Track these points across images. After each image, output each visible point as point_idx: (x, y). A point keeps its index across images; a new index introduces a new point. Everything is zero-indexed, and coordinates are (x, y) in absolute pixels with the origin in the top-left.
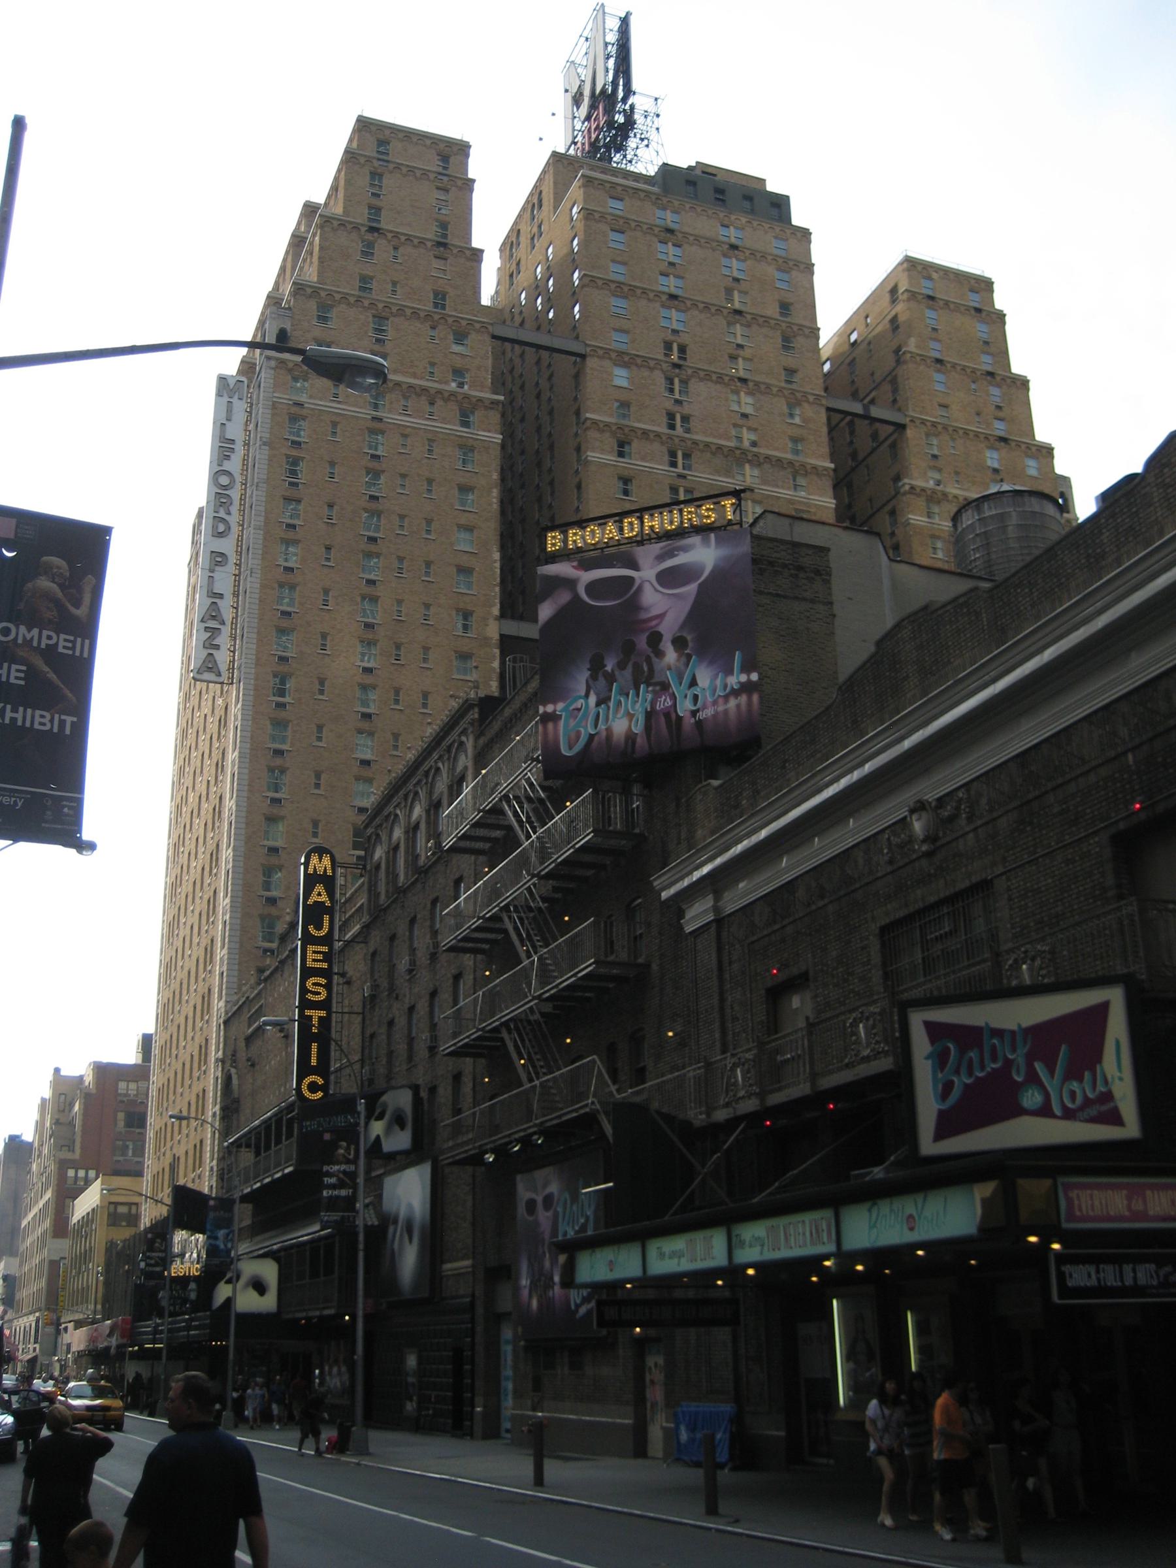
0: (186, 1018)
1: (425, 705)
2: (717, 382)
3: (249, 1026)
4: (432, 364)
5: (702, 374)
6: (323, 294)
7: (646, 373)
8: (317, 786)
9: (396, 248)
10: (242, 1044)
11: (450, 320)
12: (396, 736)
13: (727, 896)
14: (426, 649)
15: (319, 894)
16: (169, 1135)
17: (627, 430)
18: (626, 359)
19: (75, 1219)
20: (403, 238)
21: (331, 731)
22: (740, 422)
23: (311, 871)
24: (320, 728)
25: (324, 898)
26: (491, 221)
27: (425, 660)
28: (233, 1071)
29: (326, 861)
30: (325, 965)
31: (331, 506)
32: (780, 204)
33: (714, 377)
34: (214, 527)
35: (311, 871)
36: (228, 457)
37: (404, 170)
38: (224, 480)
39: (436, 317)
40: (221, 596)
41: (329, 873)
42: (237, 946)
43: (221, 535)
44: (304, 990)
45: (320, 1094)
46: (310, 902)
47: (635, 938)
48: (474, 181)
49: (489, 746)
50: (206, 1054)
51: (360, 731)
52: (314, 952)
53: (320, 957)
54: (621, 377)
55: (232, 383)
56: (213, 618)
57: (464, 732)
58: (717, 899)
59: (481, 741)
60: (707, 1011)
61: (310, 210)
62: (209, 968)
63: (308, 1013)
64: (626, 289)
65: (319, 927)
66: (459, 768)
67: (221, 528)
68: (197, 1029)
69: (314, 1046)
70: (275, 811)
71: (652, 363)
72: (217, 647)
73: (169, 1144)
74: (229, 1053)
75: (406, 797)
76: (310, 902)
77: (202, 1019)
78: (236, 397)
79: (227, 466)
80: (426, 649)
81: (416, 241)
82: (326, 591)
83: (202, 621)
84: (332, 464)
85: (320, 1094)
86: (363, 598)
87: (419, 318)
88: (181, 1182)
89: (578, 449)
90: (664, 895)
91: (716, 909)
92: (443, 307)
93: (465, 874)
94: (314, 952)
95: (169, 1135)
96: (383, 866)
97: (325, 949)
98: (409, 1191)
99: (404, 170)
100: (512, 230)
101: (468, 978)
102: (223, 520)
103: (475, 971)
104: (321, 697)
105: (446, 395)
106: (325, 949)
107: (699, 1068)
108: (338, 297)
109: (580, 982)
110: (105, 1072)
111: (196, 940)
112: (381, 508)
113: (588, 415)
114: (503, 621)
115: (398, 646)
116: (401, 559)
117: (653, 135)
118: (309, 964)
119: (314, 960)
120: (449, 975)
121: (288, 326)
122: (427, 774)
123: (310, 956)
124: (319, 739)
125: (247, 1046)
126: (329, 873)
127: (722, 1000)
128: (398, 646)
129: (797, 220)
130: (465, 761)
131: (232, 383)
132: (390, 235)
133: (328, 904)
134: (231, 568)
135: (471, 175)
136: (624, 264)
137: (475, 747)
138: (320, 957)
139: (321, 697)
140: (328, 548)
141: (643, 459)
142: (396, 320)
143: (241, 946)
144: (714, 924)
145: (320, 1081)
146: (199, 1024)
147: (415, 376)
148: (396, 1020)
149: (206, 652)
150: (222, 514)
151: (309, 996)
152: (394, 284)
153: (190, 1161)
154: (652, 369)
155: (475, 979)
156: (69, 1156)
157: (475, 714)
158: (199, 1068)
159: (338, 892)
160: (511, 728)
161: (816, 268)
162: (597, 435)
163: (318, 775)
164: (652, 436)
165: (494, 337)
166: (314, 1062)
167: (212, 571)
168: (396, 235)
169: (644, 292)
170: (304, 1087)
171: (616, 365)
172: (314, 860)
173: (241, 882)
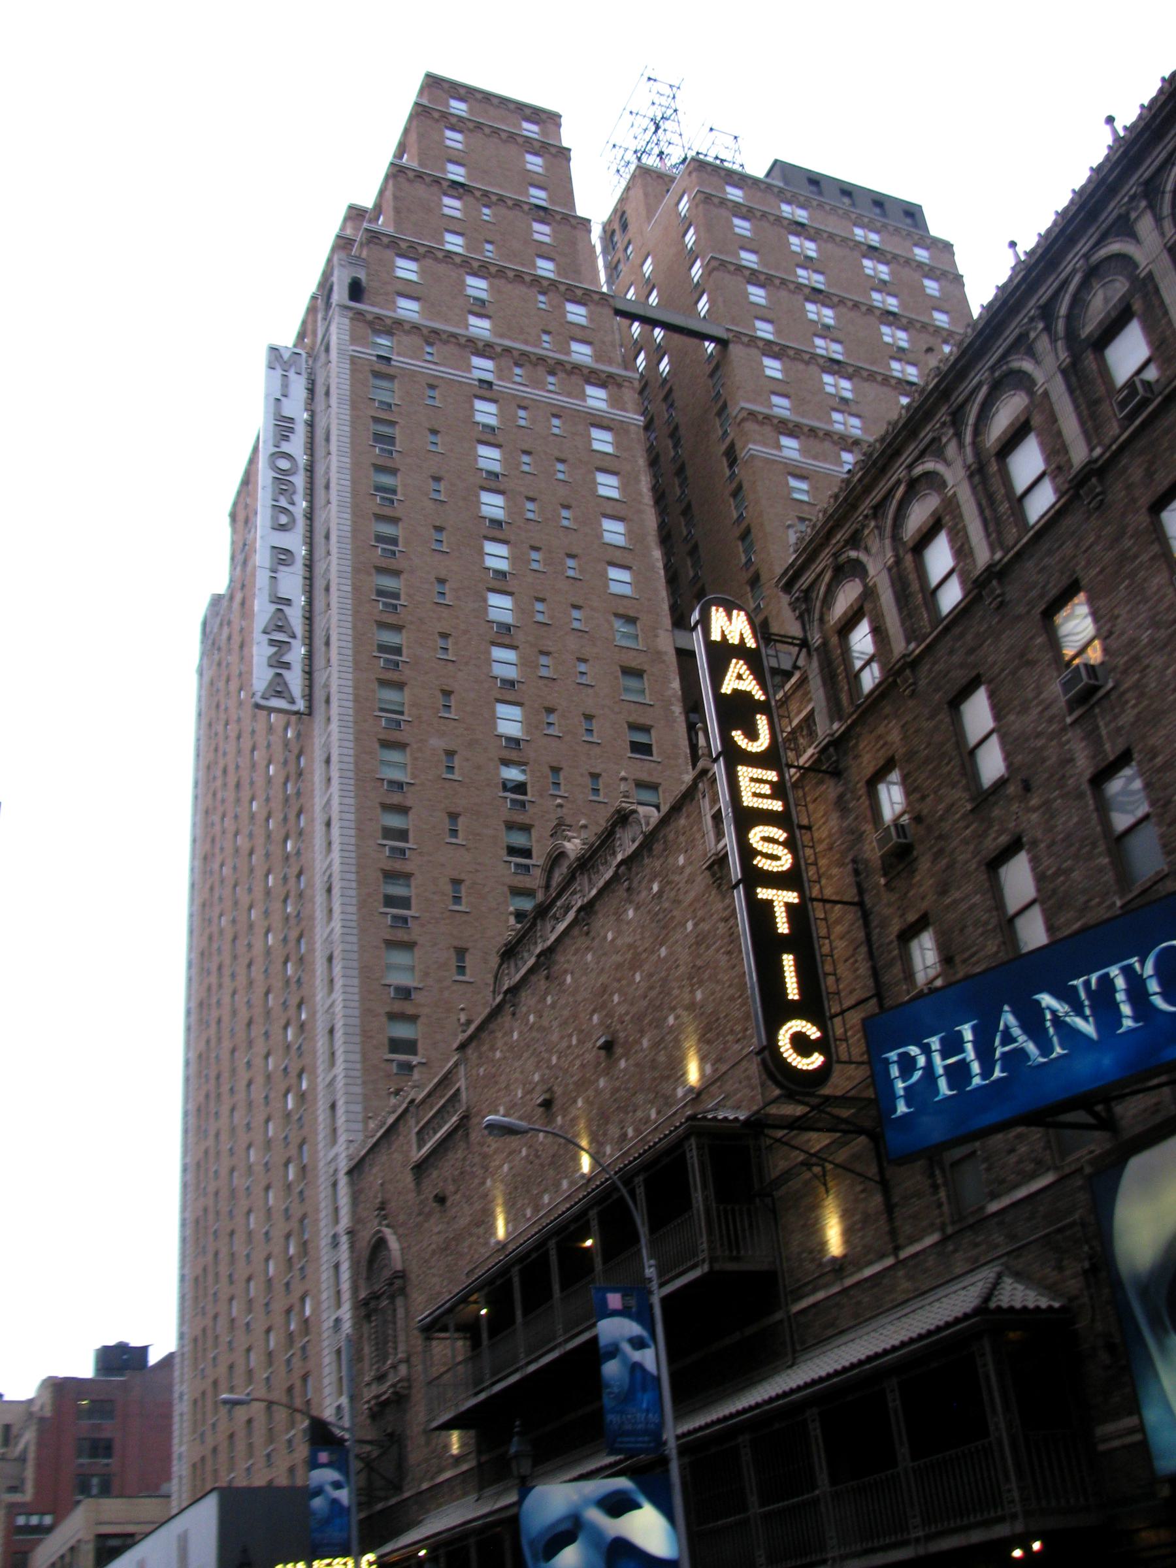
3: (421, 1143)
7: (801, 367)
8: (454, 832)
12: (556, 770)
15: (739, 677)
18: (776, 349)
32: (912, 214)
33: (879, 378)
34: (274, 518)
36: (286, 438)
37: (487, 131)
38: (284, 464)
40: (288, 602)
42: (357, 1057)
43: (282, 528)
45: (816, 1061)
48: (569, 150)
55: (286, 356)
56: (280, 629)
61: (355, 214)
63: (763, 893)
65: (753, 735)
67: (284, 519)
69: (788, 960)
70: (398, 866)
71: (806, 357)
72: (287, 666)
78: (293, 370)
79: (285, 447)
83: (265, 632)
85: (816, 1061)
94: (752, 780)
100: (615, 211)
102: (284, 510)
105: (568, 367)
107: (621, 1443)
110: (61, 1389)
112: (403, 678)
119: (755, 795)
121: (362, 275)
131: (286, 356)
134: (299, 567)
135: (565, 144)
145: (813, 1033)
147: (526, 342)
150: (283, 503)
154: (807, 363)
156: (17, 1498)
162: (756, 427)
166: (793, 991)
171: (764, 355)
173: (355, 964)
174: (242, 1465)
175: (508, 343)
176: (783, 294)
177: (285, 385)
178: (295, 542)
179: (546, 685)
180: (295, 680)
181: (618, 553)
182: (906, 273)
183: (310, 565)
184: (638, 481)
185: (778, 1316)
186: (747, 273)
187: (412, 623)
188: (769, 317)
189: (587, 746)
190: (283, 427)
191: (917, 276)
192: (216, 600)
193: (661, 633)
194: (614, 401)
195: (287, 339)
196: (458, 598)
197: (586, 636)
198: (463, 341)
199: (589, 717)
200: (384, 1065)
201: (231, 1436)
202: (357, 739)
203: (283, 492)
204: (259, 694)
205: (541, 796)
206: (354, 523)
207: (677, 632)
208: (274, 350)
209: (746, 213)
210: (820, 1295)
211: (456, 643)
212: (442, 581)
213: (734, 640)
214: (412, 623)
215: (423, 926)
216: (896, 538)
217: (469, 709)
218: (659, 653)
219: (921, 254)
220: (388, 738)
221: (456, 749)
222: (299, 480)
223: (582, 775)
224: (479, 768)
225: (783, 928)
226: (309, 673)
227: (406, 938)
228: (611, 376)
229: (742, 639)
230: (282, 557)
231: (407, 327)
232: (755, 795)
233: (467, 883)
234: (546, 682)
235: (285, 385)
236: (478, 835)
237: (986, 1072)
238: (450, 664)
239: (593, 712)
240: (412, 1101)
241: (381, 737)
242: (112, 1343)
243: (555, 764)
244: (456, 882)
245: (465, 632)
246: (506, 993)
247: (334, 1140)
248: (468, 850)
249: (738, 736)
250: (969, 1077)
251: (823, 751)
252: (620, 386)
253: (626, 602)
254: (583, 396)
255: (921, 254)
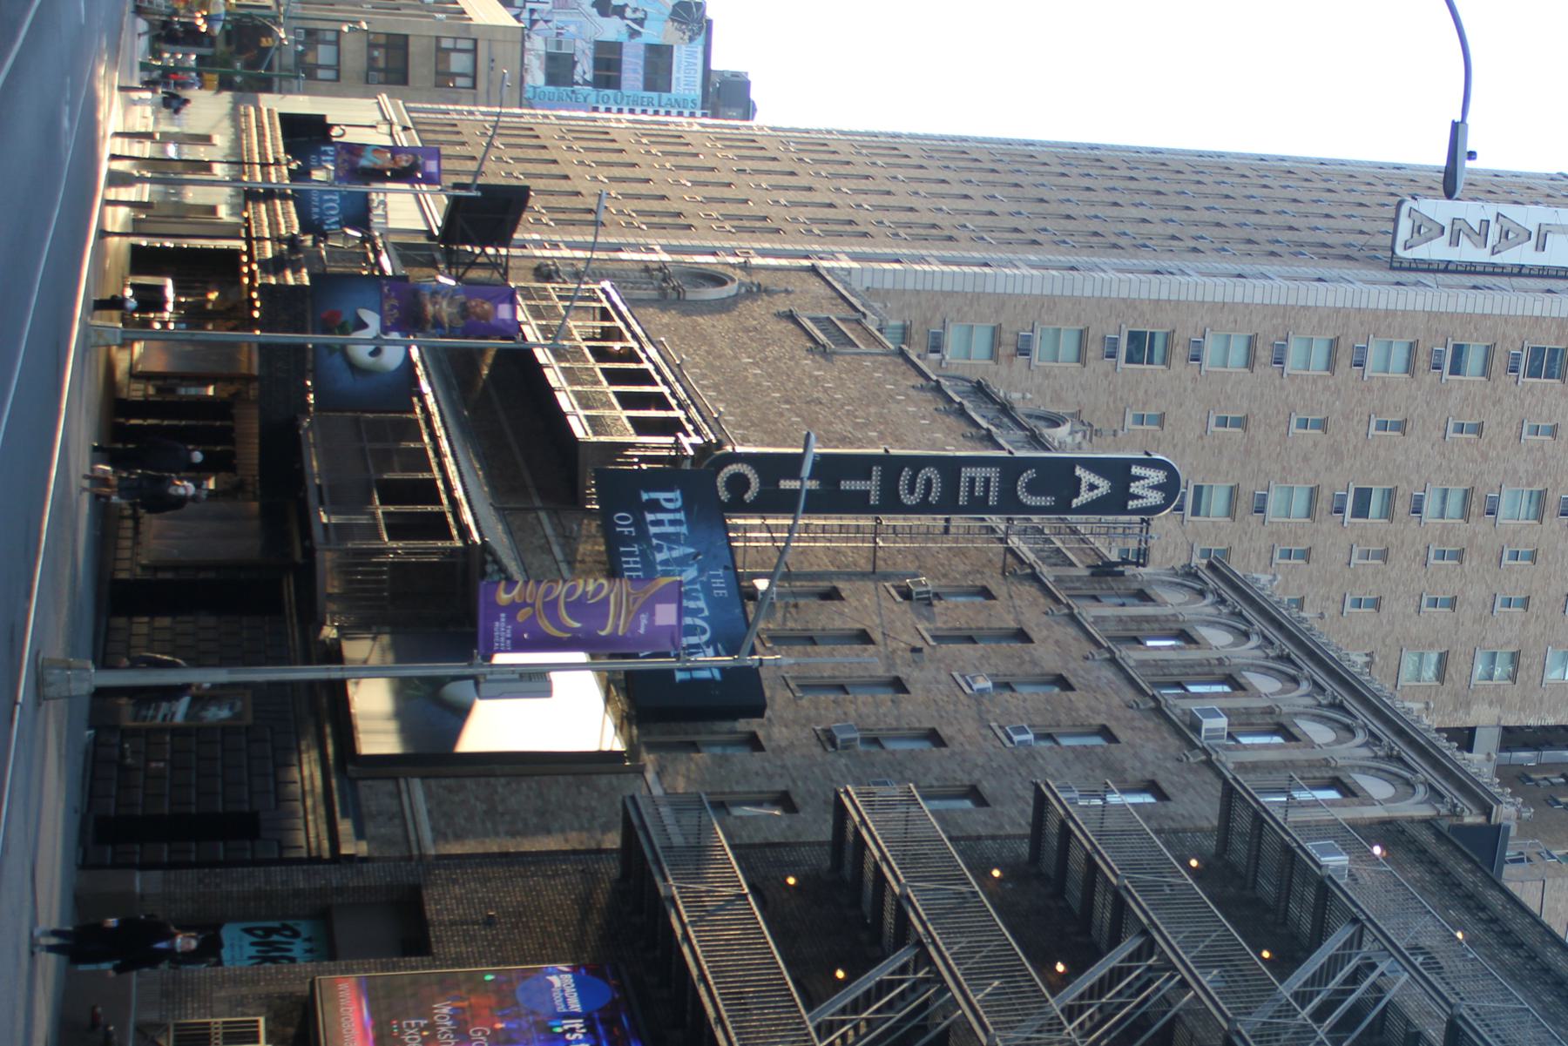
1: (1358, 603)
8: (1223, 422)
10: (782, 304)
12: (1306, 555)
14: (1452, 603)
15: (1092, 487)
16: (604, 157)
19: (1077, 912)
21: (1315, 445)
23: (1135, 470)
24: (1322, 425)
25: (1085, 496)
27: (1434, 603)
29: (1155, 498)
30: (962, 500)
35: (1135, 470)
40: (1541, 246)
41: (1132, 504)
42: (947, 287)
45: (724, 495)
46: (1079, 471)
49: (1421, 855)
50: (753, 231)
51: (1313, 494)
52: (987, 480)
53: (978, 491)
57: (1436, 795)
59: (1426, 837)
62: (901, 232)
66: (1206, 633)
68: (795, 211)
72: (1454, 242)
73: (588, 158)
77: (814, 221)
80: (1452, 603)
85: (724, 495)
88: (535, 202)
93: (1170, 805)
94: (987, 480)
95: (604, 157)
98: (559, 712)
103: (993, 838)
104: (1373, 424)
109: (850, 828)
111: (923, 189)
112: (1419, 374)
115: (1459, 556)
118: (966, 472)
120: (977, 774)
122: (1340, 707)
123: (979, 473)
124: (1304, 424)
125: (779, 315)
126: (1132, 504)
128: (1459, 556)
130: (1381, 796)
133: (1076, 502)
137: (1412, 820)
138: (978, 491)
139: (1373, 424)
148: (871, 648)
151: (906, 473)
155: (979, 838)
157: (1472, 818)
158: (728, 217)
159: (1093, 518)
160: (1468, 908)
163: (1241, 423)
172: (1157, 476)
174: (507, 154)
179: (1417, 553)
180: (1437, 250)
185: (538, 503)
187: (1494, 389)
189: (1338, 598)
193: (1496, 711)
196: (1530, 450)
197: (1487, 612)
199: (1376, 604)
200: (938, 317)
201: (566, 177)
202: (1337, 310)
204: (1415, 205)
205: (1271, 534)
207: (1496, 732)
210: (549, 531)
211: (1468, 442)
213: (1135, 488)
214: (1494, 389)
215: (1106, 375)
217: (1382, 453)
218: (1468, 705)
220: (1341, 350)
221: (1330, 433)
223: (1300, 587)
224: (1306, 459)
225: (846, 485)
226: (1447, 268)
227: (1090, 354)
232: (972, 480)
233: (1159, 433)
234: (1422, 552)
236: (1220, 452)
237: (657, 536)
238: (1441, 434)
239: (1384, 611)
240: (864, 315)
241: (1342, 340)
242: (753, 96)
243: (1313, 554)
244: (1160, 420)
245: (1485, 457)
246: (937, 382)
247: (854, 257)
248: (1201, 437)
249: (1030, 474)
250: (652, 512)
251: (1031, 566)
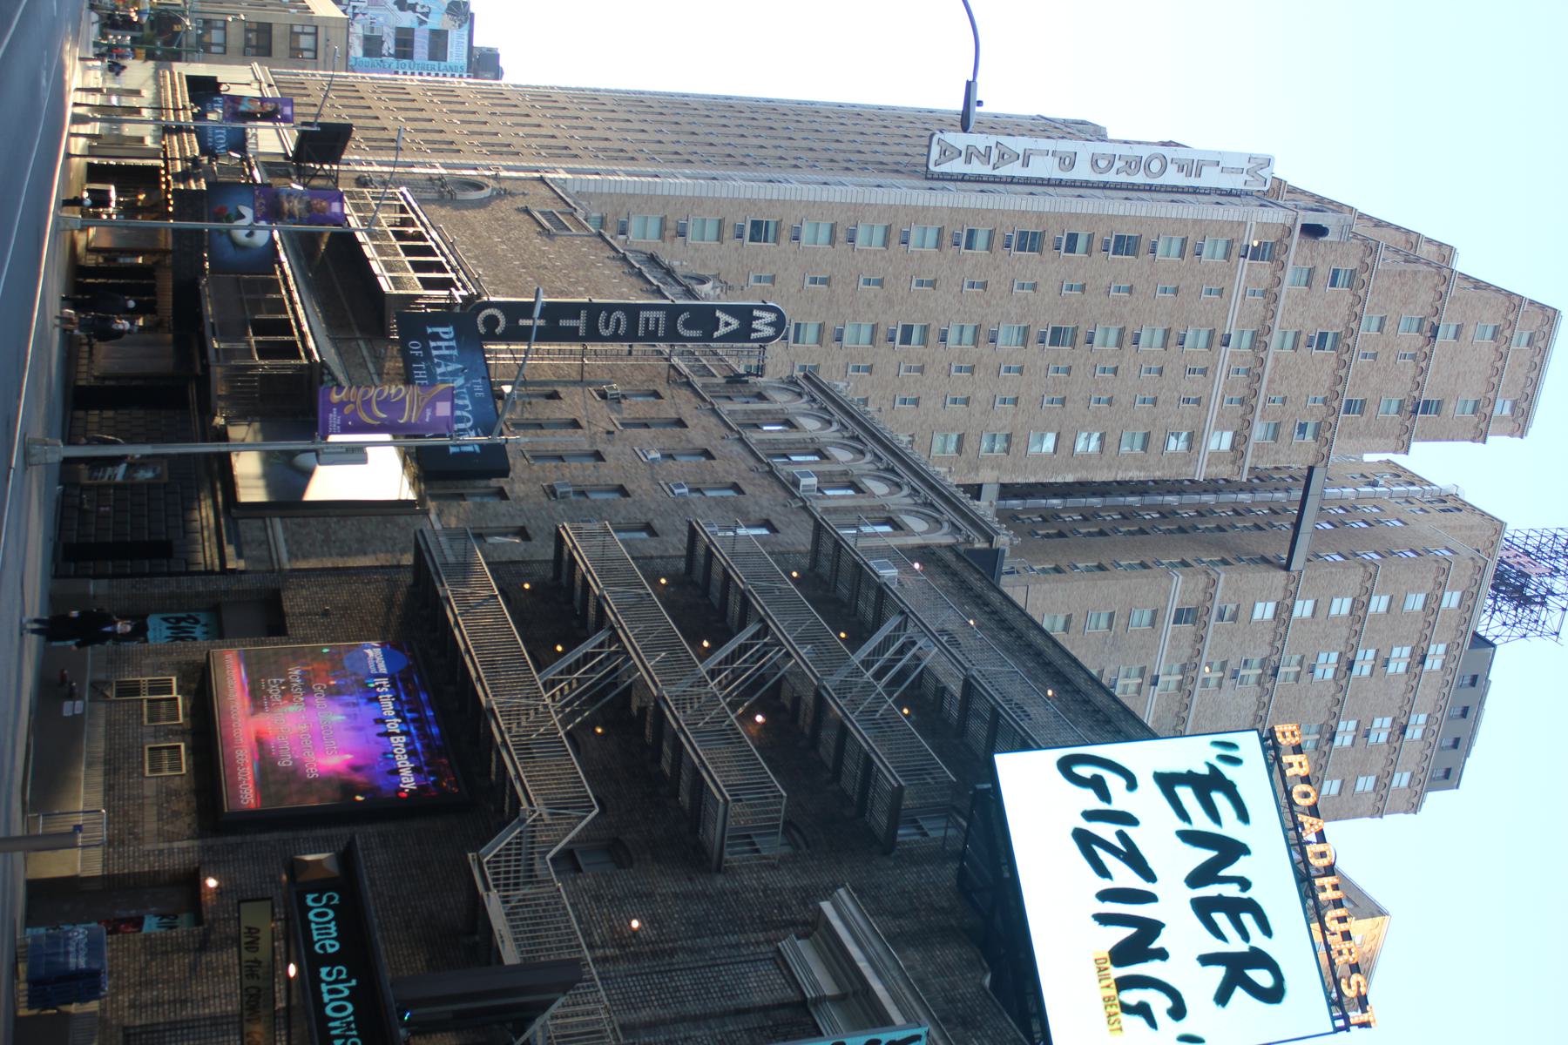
0: (553, 137)
2: (1256, 715)
3: (543, 213)
4: (1284, 401)
5: (1266, 699)
6: (1365, 276)
7: (1268, 638)
8: (814, 281)
9: (1414, 357)
10: (521, 203)
11: (1332, 419)
12: (869, 369)
13: (835, 1014)
14: (967, 401)
15: (727, 324)
16: (402, 104)
17: (1205, 618)
18: (1284, 616)
20: (1423, 365)
22: (1147, 675)
23: (756, 313)
24: (880, 283)
26: (1436, 462)
28: (486, 192)
29: (769, 331)
30: (641, 333)
31: (1130, 290)
32: (1449, 777)
35: (756, 313)
36: (1181, 169)
37: (1499, 364)
38: (1155, 166)
39: (1335, 404)
40: (1026, 164)
41: (753, 335)
42: (631, 191)
43: (1094, 163)
44: (611, 308)
45: (482, 330)
46: (718, 314)
47: (749, 836)
49: (946, 569)
52: (657, 320)
54: (1264, 611)
57: (956, 529)
58: (834, 1000)
59: (949, 557)
60: (677, 989)
63: (583, 313)
64: (1361, 613)
67: (1102, 164)
68: (529, 140)
71: (1278, 644)
72: (968, 161)
73: (392, 105)
74: (506, 185)
75: (856, 438)
76: (718, 314)
77: (542, 147)
80: (967, 401)
81: (1420, 379)
82: (1034, 287)
84: (1176, 291)
85: (482, 330)
86: (1026, 329)
87: (1335, 384)
88: (357, 135)
89: (1184, 564)
90: (826, 906)
91: (820, 1000)
92: (1347, 411)
94: (657, 320)
95: (402, 104)
96: (764, 406)
97: (661, 333)
98: (375, 474)
99: (1499, 364)
101: (649, 546)
103: (661, 557)
106: (661, 333)
108: (1361, 293)
109: (578, 577)
113: (1223, 576)
114: (996, 487)
116: (1068, 370)
117: (1518, 631)
118: (643, 314)
119: (647, 320)
120: (651, 515)
122: (892, 471)
123: (652, 315)
124: (868, 282)
126: (753, 335)
127: (696, 1019)
128: (971, 370)
129: (1432, 797)
131: (1265, 173)
132: (1427, 349)
133: (716, 334)
136: (1388, 610)
137: (940, 546)
140: (1083, 288)
141: (1173, 637)
142: (1333, 360)
143: (633, 195)
144: (798, 998)
145: (498, 330)
146: (534, 142)
147: (1271, 381)
149: (963, 149)
150: (1118, 164)
152: (1375, 356)
153: (375, 134)
154: (1272, 644)
155: (652, 557)
157: (980, 544)
158: (484, 144)
160: (977, 605)
161: (1377, 820)
162: (1201, 586)
163: (826, 281)
164: (1198, 646)
165: (1311, 469)
167: (1054, 153)
168: (1427, 357)
169: (1357, 633)
170: (488, 312)
175: (1269, 364)
176: (1345, 632)
177: (1233, 171)
178: (1082, 172)
180: (957, 166)
181: (1069, 443)
182: (1380, 762)
183: (1060, 183)
184: (1141, 468)
186: (1364, 599)
188: (1318, 613)
190: (1193, 167)
191: (1378, 770)
192: (1446, 252)
193: (996, 473)
194: (1216, 456)
195: (1280, 171)
196: (1019, 300)
198: (1268, 323)
203: (1128, 164)
206: (1085, 215)
208: (1269, 162)
209: (1432, 605)
212: (1034, 287)
216: (832, 444)
219: (1401, 779)
222: (1140, 178)
226: (963, 178)
228: (1243, 455)
229: (756, 331)
230: (1068, 161)
231: (1279, 274)
232: (647, 320)
235: (1233, 171)
242: (502, 64)
245: (988, 304)
249: (686, 315)
252: (1234, 462)
253: (1023, 445)
254: (1221, 427)
255: (1401, 779)
